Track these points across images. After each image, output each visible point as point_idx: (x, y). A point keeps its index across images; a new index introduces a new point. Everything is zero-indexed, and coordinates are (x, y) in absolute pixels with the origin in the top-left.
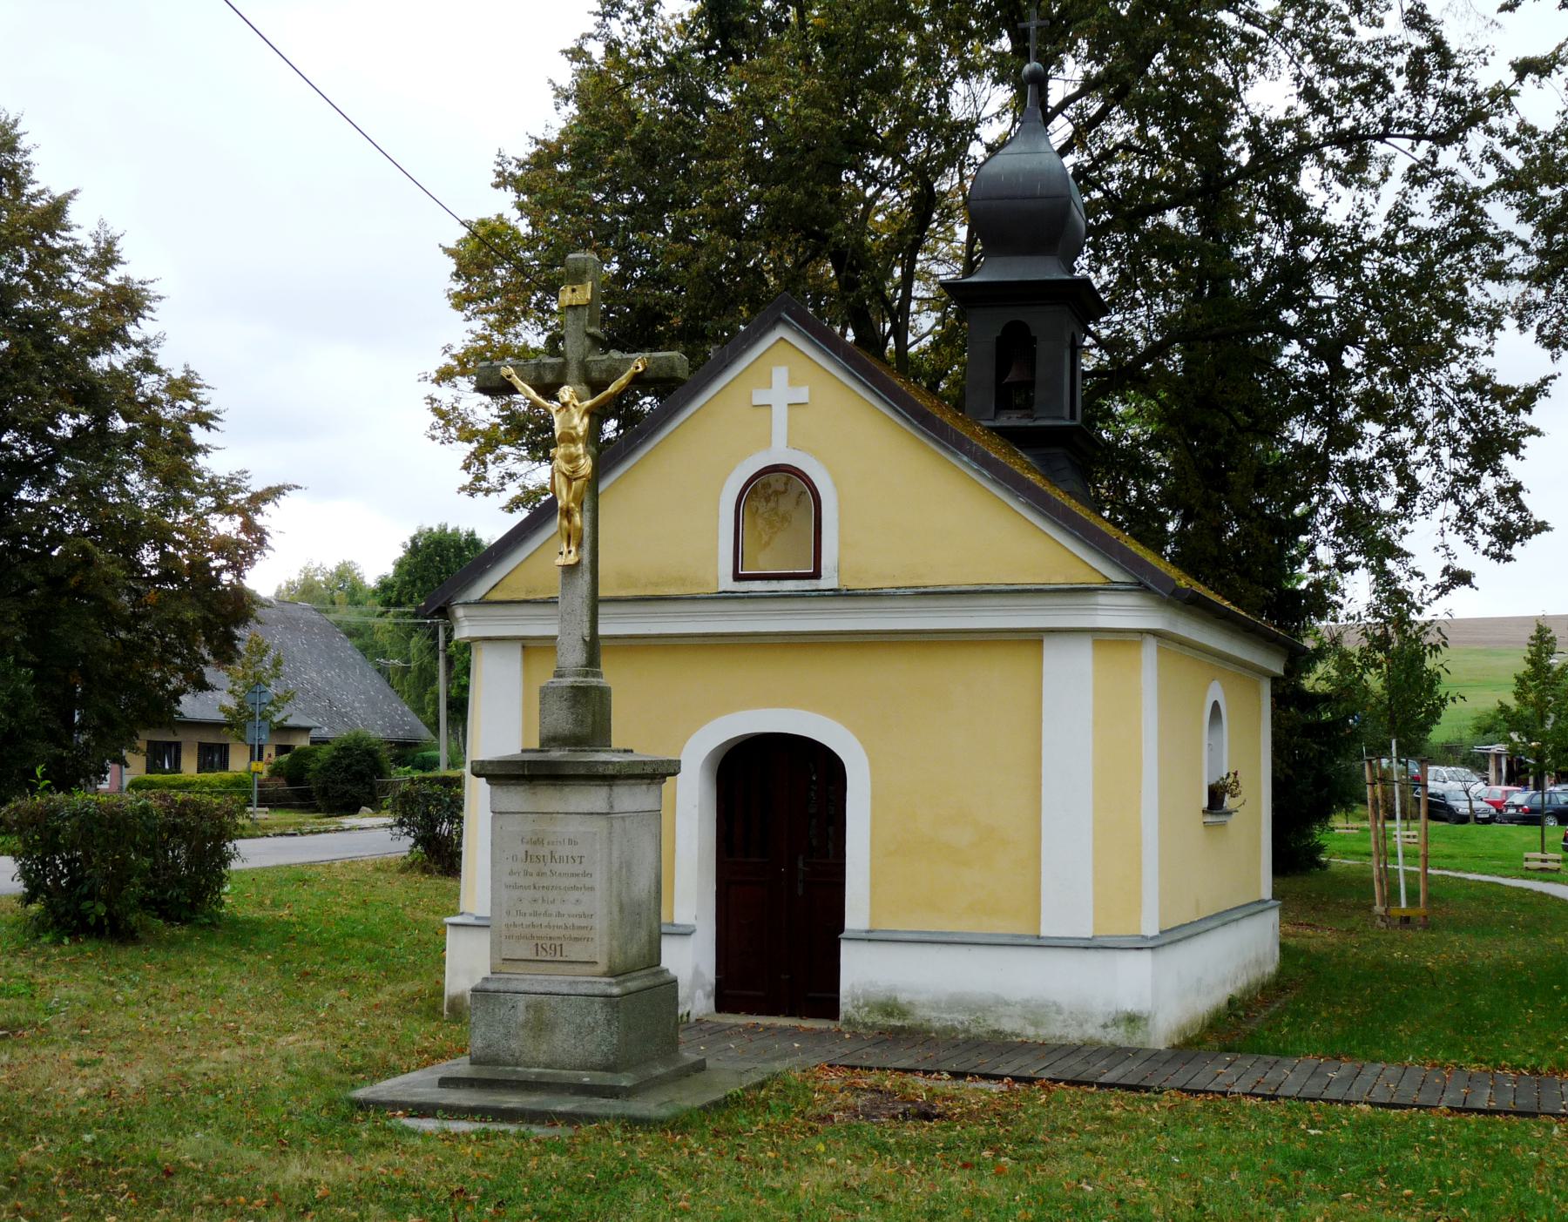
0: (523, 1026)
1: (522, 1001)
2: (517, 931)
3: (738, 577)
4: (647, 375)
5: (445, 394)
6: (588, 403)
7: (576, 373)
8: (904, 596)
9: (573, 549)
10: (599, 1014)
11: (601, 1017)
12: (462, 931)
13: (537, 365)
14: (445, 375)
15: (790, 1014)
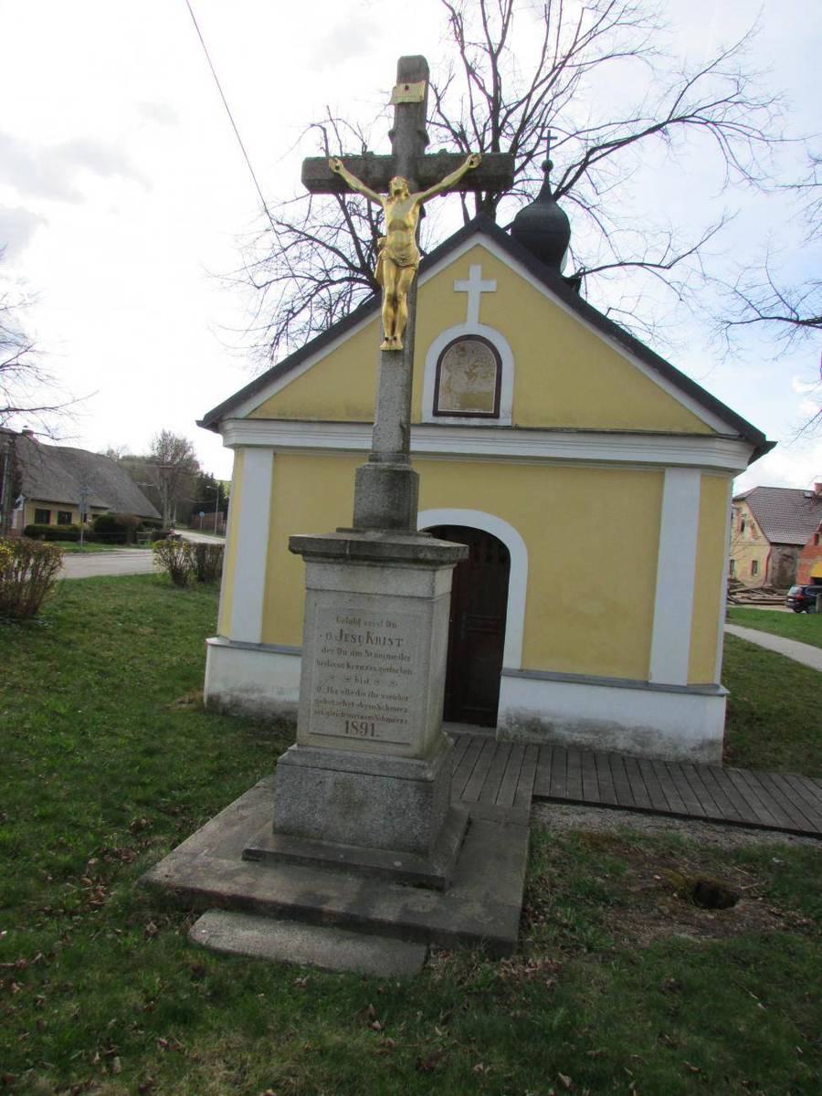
0: (331, 802)
1: (330, 778)
3: (436, 413)
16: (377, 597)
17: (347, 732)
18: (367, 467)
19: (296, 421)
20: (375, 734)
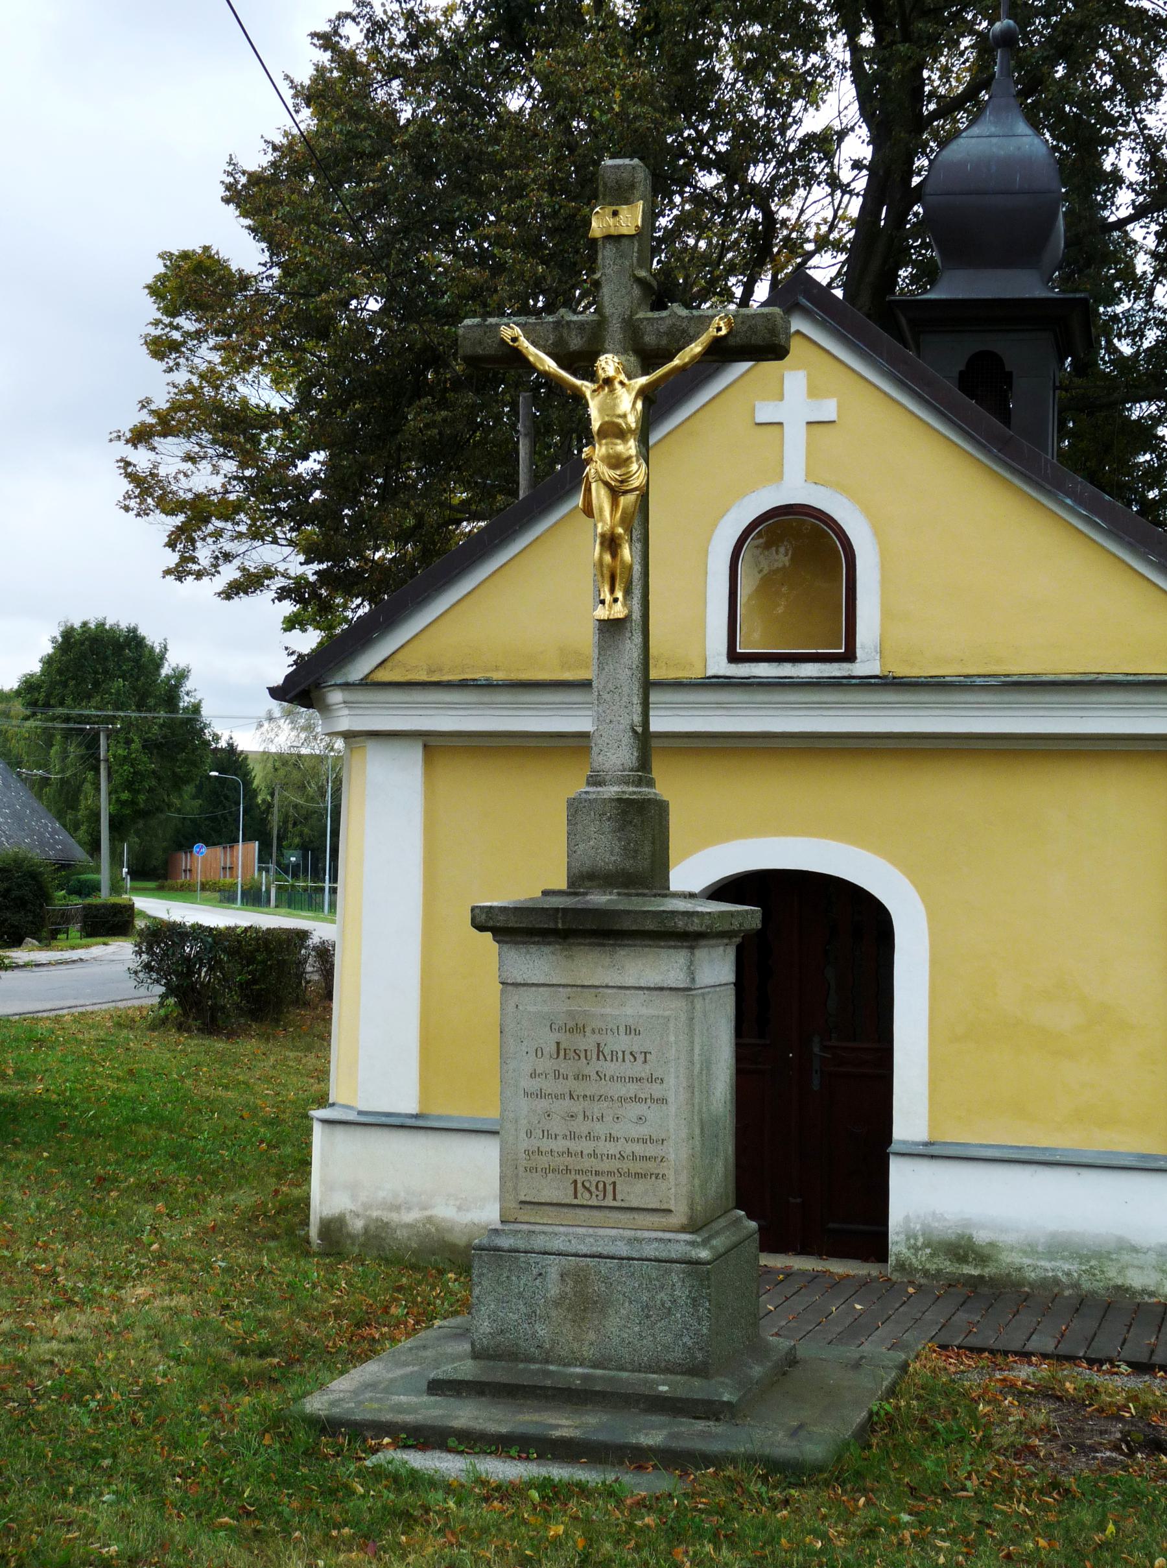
0: (557, 1304)
1: (553, 1268)
2: (543, 1161)
3: (734, 657)
4: (732, 341)
5: (142, 458)
6: (643, 380)
7: (619, 336)
8: (985, 688)
9: (619, 594)
10: (679, 1287)
11: (681, 1293)
12: (340, 1133)
13: (558, 324)
14: (141, 436)
15: (804, 1250)
16: (609, 991)
17: (576, 1197)
18: (584, 796)
19: (463, 685)
20: (619, 1197)
